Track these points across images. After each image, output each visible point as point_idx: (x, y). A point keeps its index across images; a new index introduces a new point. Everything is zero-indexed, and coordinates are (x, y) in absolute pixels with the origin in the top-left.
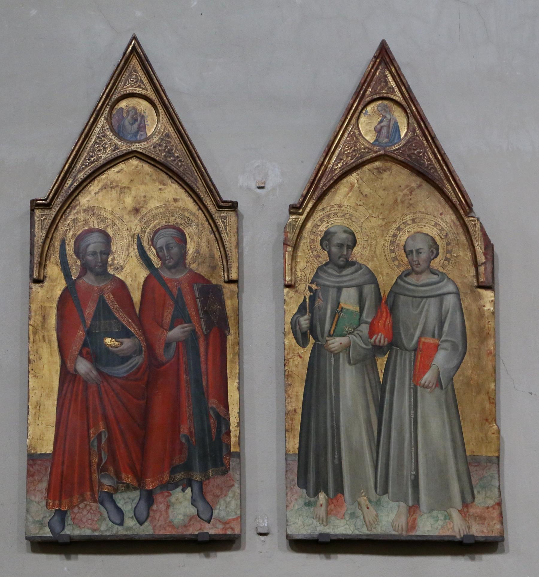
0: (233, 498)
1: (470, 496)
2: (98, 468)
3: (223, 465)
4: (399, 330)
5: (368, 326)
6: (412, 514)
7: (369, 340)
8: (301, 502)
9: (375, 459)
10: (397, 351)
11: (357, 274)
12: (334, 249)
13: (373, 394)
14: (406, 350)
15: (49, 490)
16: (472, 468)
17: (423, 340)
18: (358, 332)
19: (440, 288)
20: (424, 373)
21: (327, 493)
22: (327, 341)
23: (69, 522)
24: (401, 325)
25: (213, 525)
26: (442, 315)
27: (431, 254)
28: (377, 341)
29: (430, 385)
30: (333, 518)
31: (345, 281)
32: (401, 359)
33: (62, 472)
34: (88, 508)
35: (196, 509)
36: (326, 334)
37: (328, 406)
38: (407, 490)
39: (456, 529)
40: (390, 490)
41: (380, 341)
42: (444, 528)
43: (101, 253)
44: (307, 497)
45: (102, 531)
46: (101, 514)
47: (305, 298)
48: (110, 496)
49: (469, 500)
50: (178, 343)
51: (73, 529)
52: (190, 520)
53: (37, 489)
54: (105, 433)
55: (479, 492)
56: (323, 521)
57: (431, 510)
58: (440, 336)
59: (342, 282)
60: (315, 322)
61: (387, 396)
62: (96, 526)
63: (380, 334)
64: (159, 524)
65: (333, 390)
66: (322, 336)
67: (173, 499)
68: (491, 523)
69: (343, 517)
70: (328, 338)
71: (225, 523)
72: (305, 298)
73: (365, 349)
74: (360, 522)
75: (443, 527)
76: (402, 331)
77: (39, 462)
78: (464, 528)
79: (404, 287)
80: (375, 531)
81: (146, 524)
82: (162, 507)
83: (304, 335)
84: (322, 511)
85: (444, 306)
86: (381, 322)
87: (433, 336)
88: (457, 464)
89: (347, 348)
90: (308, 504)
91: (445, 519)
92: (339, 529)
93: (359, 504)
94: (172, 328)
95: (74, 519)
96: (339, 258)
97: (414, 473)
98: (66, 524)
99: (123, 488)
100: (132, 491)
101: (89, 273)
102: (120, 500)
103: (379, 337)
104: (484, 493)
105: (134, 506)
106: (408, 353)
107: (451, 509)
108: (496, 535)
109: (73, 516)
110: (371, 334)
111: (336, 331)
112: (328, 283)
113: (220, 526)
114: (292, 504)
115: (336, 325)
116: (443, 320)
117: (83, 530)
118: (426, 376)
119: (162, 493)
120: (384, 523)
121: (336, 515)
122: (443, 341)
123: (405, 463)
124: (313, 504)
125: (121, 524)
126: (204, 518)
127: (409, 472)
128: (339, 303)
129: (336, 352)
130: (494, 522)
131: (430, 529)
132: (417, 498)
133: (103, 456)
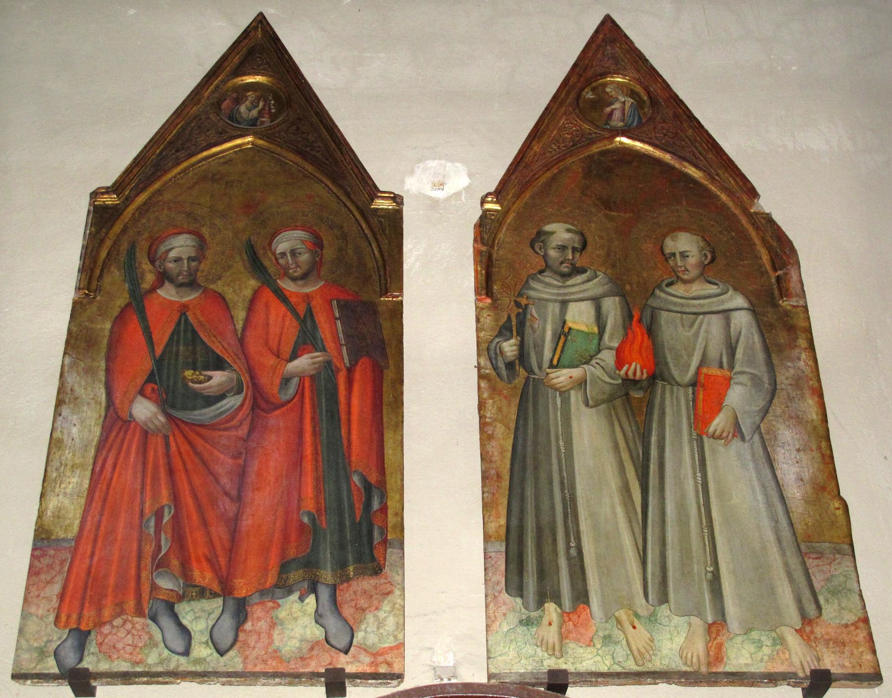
0: (390, 612)
1: (813, 607)
2: (154, 559)
3: (373, 559)
4: (665, 358)
5: (614, 352)
6: (714, 636)
7: (617, 372)
8: (513, 619)
9: (641, 548)
10: (664, 386)
11: (591, 283)
12: (553, 253)
13: (630, 450)
14: (679, 384)
15: (62, 597)
16: (809, 562)
17: (704, 370)
18: (598, 361)
19: (723, 302)
20: (712, 418)
21: (559, 605)
22: (548, 374)
23: (92, 650)
24: (667, 352)
25: (354, 657)
26: (730, 337)
27: (703, 258)
28: (630, 373)
29: (725, 434)
30: (572, 645)
31: (573, 293)
32: (672, 396)
33: (90, 566)
34: (129, 626)
35: (323, 630)
36: (546, 364)
37: (555, 467)
38: (703, 594)
39: (796, 661)
40: (671, 596)
41: (635, 373)
42: (774, 659)
43: (190, 259)
44: (523, 610)
45: (150, 665)
46: (151, 637)
47: (509, 318)
48: (170, 608)
49: (811, 613)
50: (302, 379)
51: (99, 661)
52: (312, 649)
53: (42, 595)
54: (170, 507)
55: (827, 600)
56: (554, 649)
57: (748, 631)
58: (731, 367)
59: (566, 294)
60: (526, 347)
61: (654, 452)
62: (140, 657)
63: (634, 364)
64: (254, 653)
65: (561, 443)
66: (540, 368)
67: (282, 614)
68: (855, 651)
69: (590, 643)
70: (549, 371)
71: (375, 655)
72: (509, 318)
73: (611, 384)
74: (621, 652)
75: (771, 658)
76: (669, 360)
77: (52, 552)
78: (809, 659)
79: (666, 300)
80: (650, 665)
81: (232, 653)
82: (263, 625)
83: (510, 365)
84: (551, 634)
85: (732, 325)
86: (636, 346)
87: (721, 366)
88: (783, 554)
89: (582, 383)
90: (527, 622)
91: (774, 644)
92: (584, 664)
93: (619, 622)
94: (294, 356)
95: (101, 644)
96: (562, 263)
97: (711, 569)
98: (86, 653)
99: (194, 594)
100: (209, 598)
101: (167, 284)
102: (187, 613)
103: (633, 367)
104: (836, 601)
105: (211, 623)
106: (682, 391)
107: (783, 628)
108: (867, 671)
109: (100, 639)
110: (619, 364)
111: (562, 360)
112: (546, 296)
113: (367, 659)
114: (498, 623)
115: (562, 352)
116: (733, 345)
117: (116, 663)
118: (716, 422)
119: (262, 603)
120: (665, 652)
121: (577, 640)
122: (736, 374)
123: (694, 548)
124: (536, 622)
125: (186, 653)
126: (338, 646)
127: (703, 568)
128: (564, 322)
129: (564, 389)
130: (861, 649)
131: (749, 661)
132: (721, 611)
133: (163, 542)
